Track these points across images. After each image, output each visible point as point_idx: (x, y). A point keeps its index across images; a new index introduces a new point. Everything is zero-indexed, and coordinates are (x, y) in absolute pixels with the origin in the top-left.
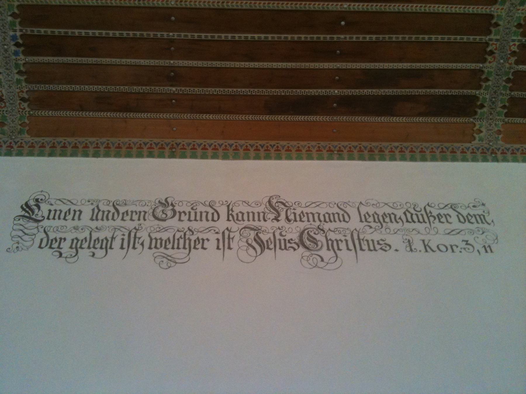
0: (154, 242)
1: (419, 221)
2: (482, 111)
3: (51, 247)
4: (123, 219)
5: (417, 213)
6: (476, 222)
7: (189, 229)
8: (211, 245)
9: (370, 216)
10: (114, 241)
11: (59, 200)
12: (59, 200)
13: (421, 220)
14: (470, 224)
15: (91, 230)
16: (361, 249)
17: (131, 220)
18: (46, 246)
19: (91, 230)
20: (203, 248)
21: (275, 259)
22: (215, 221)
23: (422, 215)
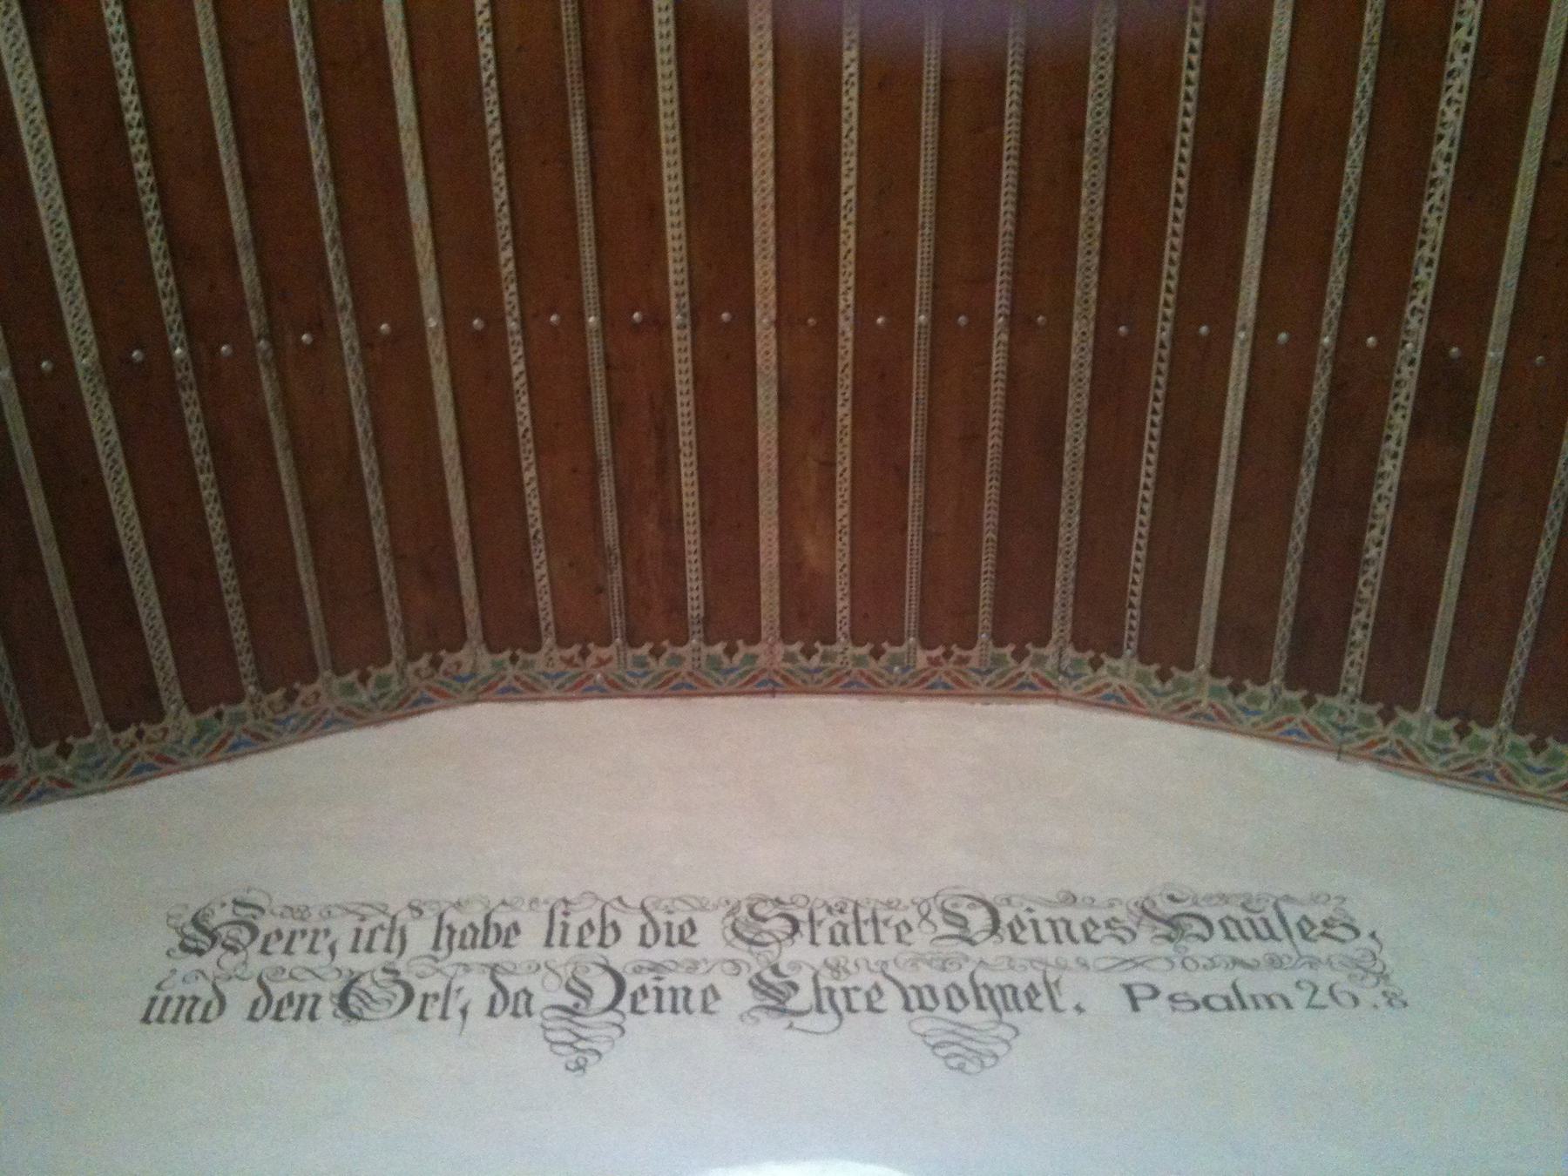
0: (912, 995)
1: (1259, 936)
2: (1009, 658)
3: (277, 1018)
4: (264, 951)
5: (1253, 916)
6: (1053, 938)
7: (1078, 960)
8: (326, 1008)
9: (1097, 927)
10: (1060, 995)
11: (680, 899)
12: (680, 899)
13: (1264, 932)
14: (689, 949)
15: (1042, 967)
16: (850, 1009)
17: (312, 950)
18: (504, 1009)
19: (1042, 967)
20: (871, 1008)
21: (460, 1034)
22: (649, 946)
23: (1266, 922)
